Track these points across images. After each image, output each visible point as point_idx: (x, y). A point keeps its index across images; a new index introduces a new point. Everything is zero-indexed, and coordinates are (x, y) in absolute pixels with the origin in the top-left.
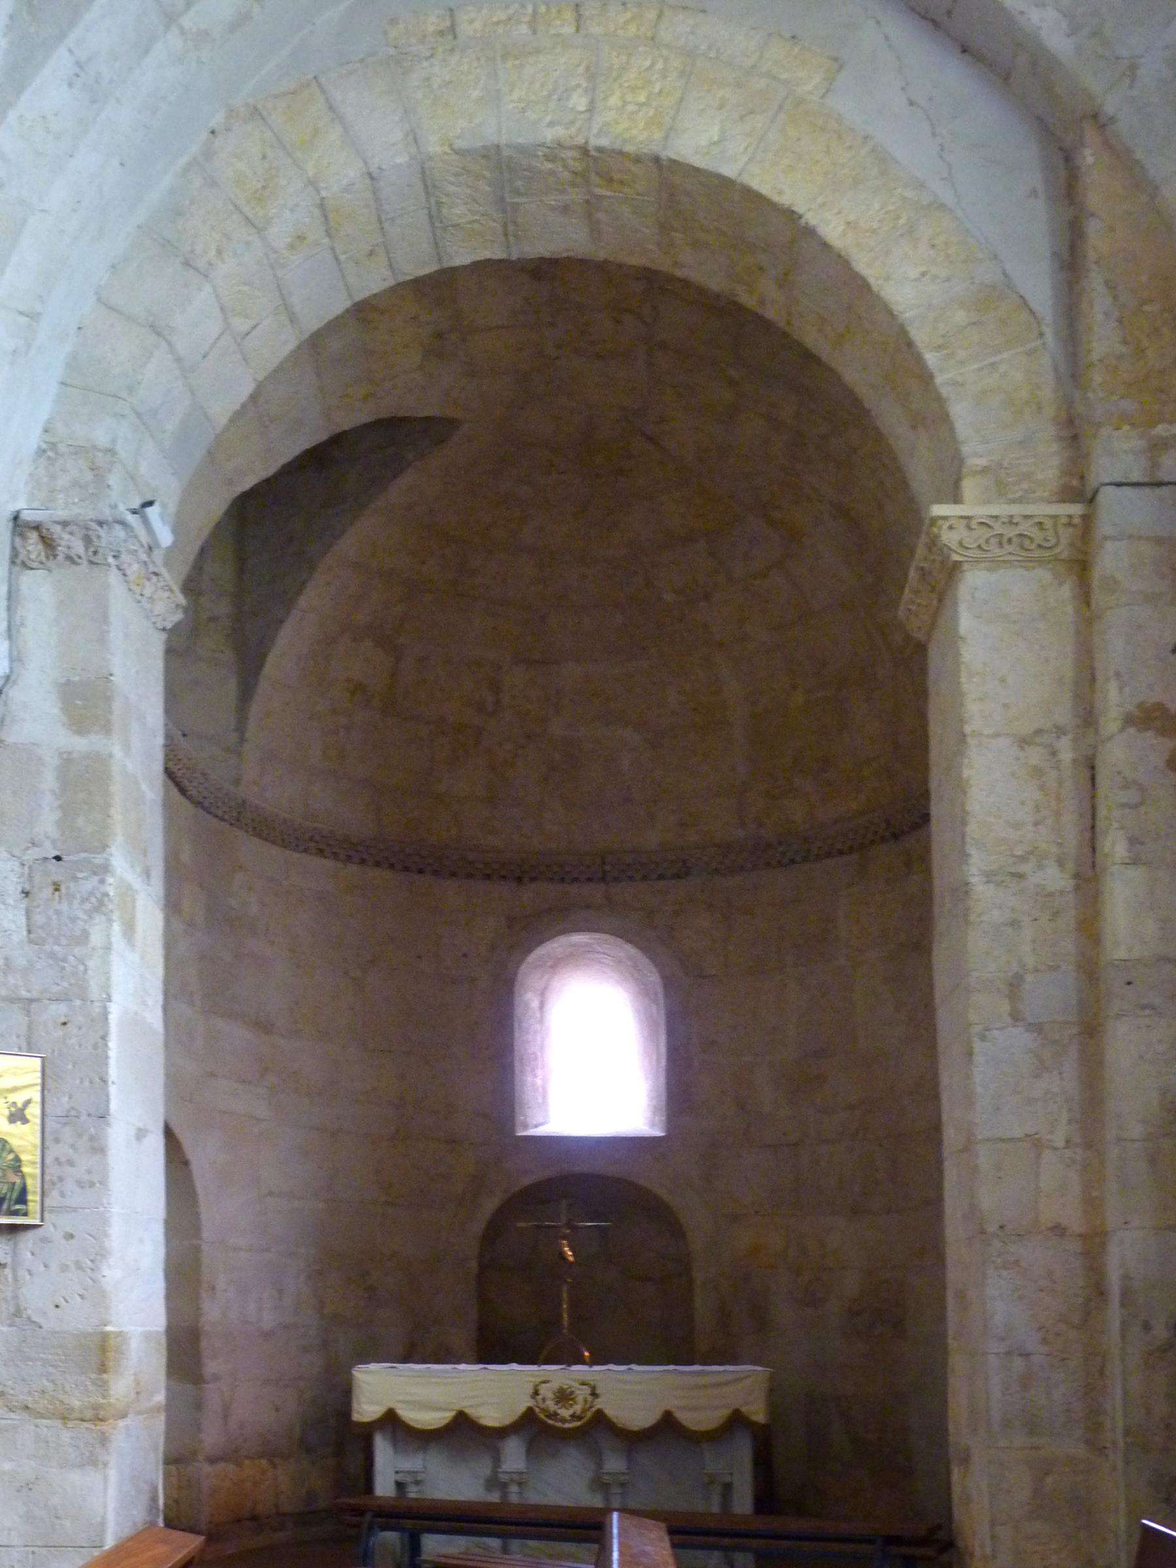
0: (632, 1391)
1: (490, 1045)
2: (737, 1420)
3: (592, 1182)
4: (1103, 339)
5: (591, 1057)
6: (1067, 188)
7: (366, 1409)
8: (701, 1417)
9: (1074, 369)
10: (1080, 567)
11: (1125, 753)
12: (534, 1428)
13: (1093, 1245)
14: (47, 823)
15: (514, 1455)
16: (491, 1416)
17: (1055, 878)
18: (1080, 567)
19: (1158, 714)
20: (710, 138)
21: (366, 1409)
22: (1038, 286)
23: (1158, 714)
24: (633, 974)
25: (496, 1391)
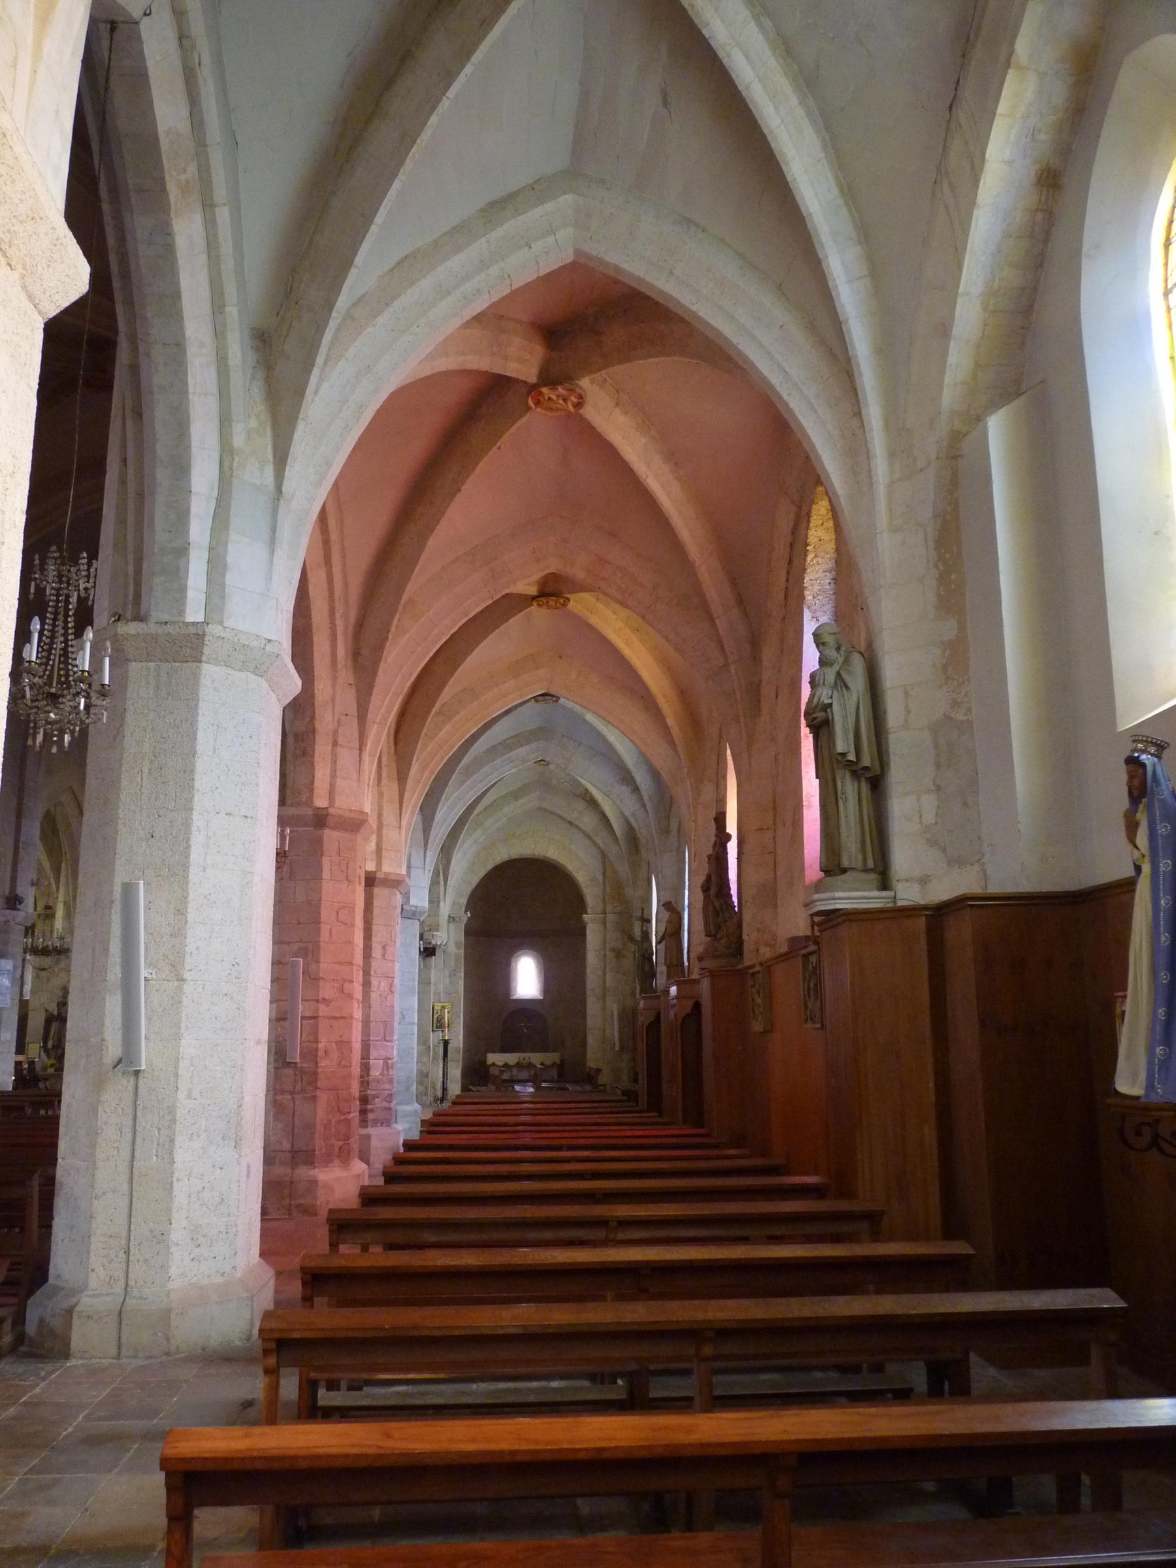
0: (536, 1058)
1: (505, 978)
2: (554, 1064)
3: (526, 1008)
4: (608, 890)
5: (527, 978)
6: (604, 863)
7: (489, 1062)
8: (548, 1063)
9: (604, 892)
10: (604, 924)
11: (610, 955)
12: (519, 1065)
13: (604, 1031)
14: (453, 964)
15: (515, 1072)
16: (511, 1063)
17: (600, 973)
18: (604, 924)
19: (544, 1085)
20: (552, 853)
21: (489, 1062)
22: (600, 878)
23: (544, 1085)
24: (535, 958)
25: (511, 1058)
